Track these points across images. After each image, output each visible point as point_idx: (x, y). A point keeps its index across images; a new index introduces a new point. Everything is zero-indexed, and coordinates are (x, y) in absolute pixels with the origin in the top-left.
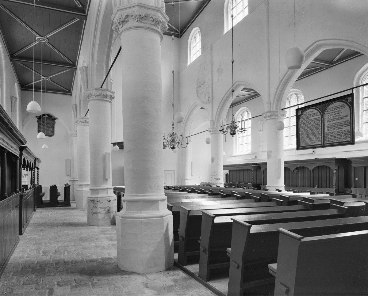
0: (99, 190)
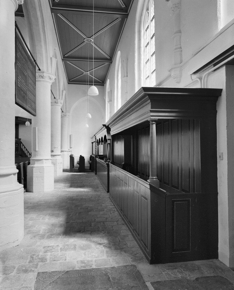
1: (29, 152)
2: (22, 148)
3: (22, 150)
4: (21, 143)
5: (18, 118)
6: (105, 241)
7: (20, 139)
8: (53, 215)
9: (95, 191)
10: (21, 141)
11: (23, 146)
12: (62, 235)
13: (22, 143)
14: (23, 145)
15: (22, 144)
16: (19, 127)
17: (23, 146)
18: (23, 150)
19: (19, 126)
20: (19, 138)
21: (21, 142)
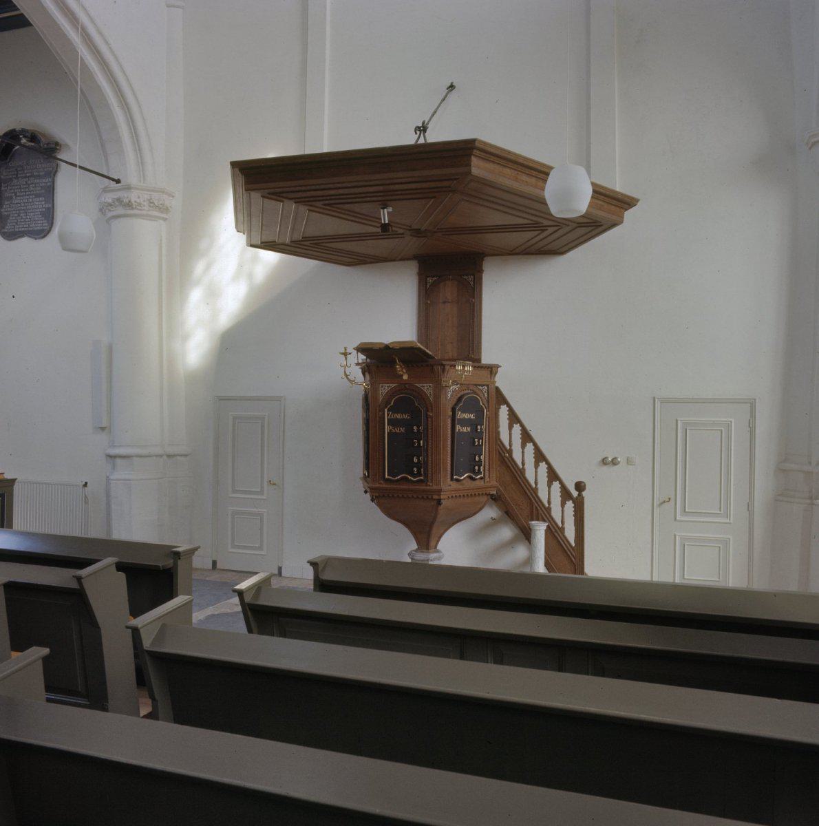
0: (135, 458)
1: (518, 421)
2: (504, 437)
3: (504, 457)
4: (501, 399)
5: (474, 160)
6: (416, 261)
7: (492, 370)
8: (284, 587)
9: (550, 572)
10: (500, 381)
11: (536, 466)
12: (200, 561)
13: (506, 402)
14: (514, 418)
15: (503, 411)
16: (481, 279)
17: (517, 428)
18: (517, 456)
19: (481, 271)
20: (486, 359)
21: (497, 389)
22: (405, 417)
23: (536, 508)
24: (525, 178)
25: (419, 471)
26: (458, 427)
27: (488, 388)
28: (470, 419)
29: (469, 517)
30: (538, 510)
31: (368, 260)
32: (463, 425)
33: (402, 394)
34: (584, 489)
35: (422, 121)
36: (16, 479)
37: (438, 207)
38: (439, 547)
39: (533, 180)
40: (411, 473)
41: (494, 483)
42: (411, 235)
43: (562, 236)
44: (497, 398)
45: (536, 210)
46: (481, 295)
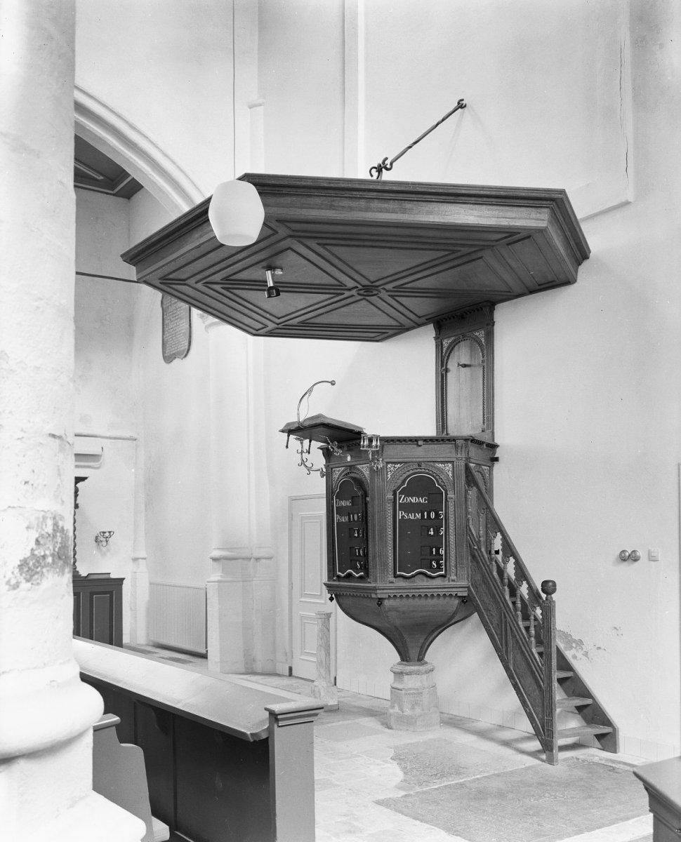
22: (422, 501)
23: (504, 614)
24: (346, 203)
25: (439, 565)
26: (400, 514)
27: (453, 465)
28: (347, 507)
29: (360, 622)
30: (505, 617)
31: (391, 332)
32: (408, 512)
33: (435, 478)
34: (554, 591)
35: (384, 157)
36: (124, 579)
37: (564, 219)
38: (427, 658)
39: (363, 203)
40: (430, 568)
41: (465, 583)
42: (8, 357)
43: (206, 294)
44: (467, 477)
45: (201, 271)
46: (493, 342)
